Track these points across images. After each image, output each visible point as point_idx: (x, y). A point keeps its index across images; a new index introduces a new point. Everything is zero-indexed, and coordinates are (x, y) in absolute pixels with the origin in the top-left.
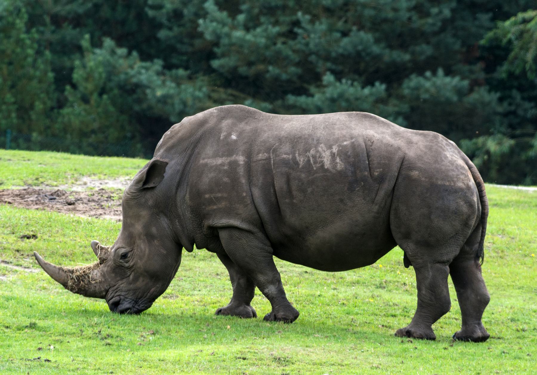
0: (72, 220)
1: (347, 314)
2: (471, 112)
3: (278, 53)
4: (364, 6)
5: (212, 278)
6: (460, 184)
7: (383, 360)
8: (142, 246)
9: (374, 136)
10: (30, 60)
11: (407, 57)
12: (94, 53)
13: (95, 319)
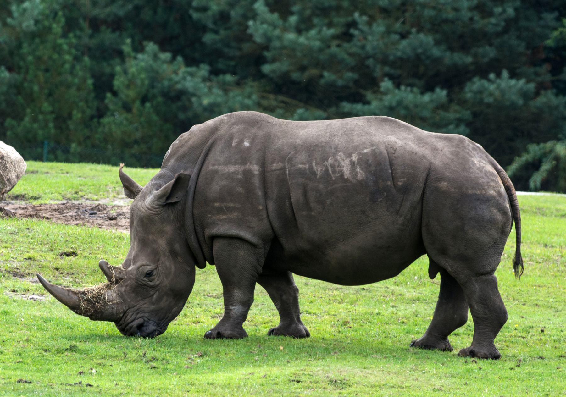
0: (113, 236)
1: (407, 333)
2: (537, 117)
3: (333, 57)
4: (423, 6)
5: (263, 295)
7: (446, 382)
8: (167, 263)
9: (396, 143)
10: (67, 66)
11: (469, 59)
12: (135, 58)
13: (140, 341)
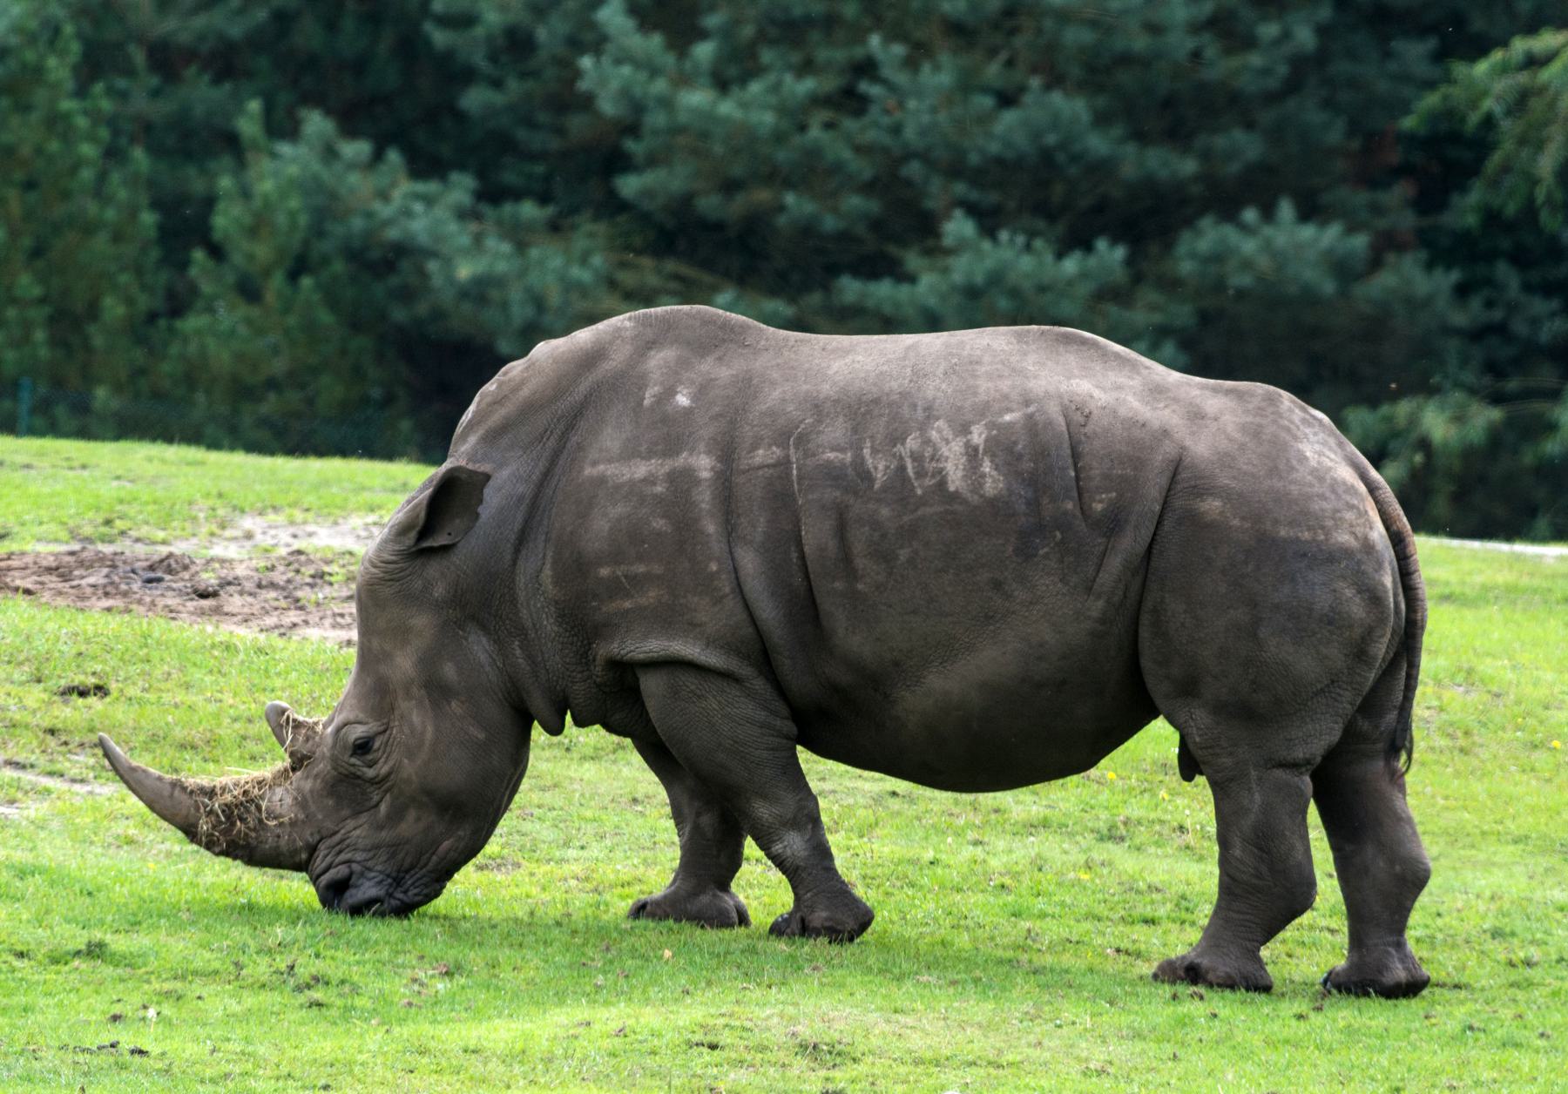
0: (209, 641)
1: (1014, 915)
2: (1375, 326)
3: (813, 154)
4: (1064, 17)
5: (618, 811)
6: (1344, 538)
7: (1119, 1050)
8: (416, 718)
9: (1092, 397)
10: (87, 175)
11: (1188, 166)
12: (274, 155)
13: (279, 930)
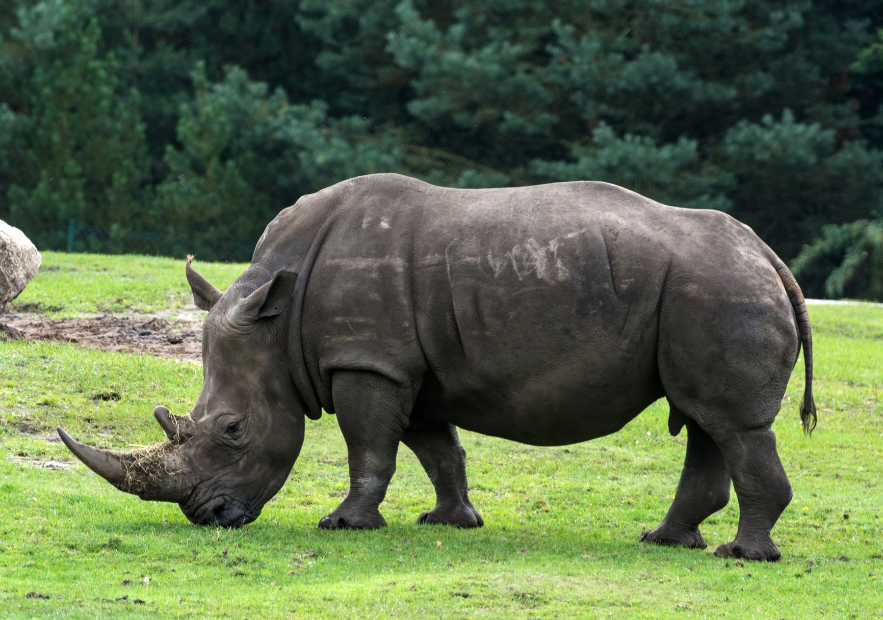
0: (177, 368)
1: (636, 520)
2: (838, 183)
3: (520, 89)
4: (661, 9)
5: (410, 461)
6: (767, 300)
7: (696, 596)
8: (261, 411)
9: (618, 223)
10: (105, 103)
11: (732, 93)
12: (211, 91)
13: (218, 532)
